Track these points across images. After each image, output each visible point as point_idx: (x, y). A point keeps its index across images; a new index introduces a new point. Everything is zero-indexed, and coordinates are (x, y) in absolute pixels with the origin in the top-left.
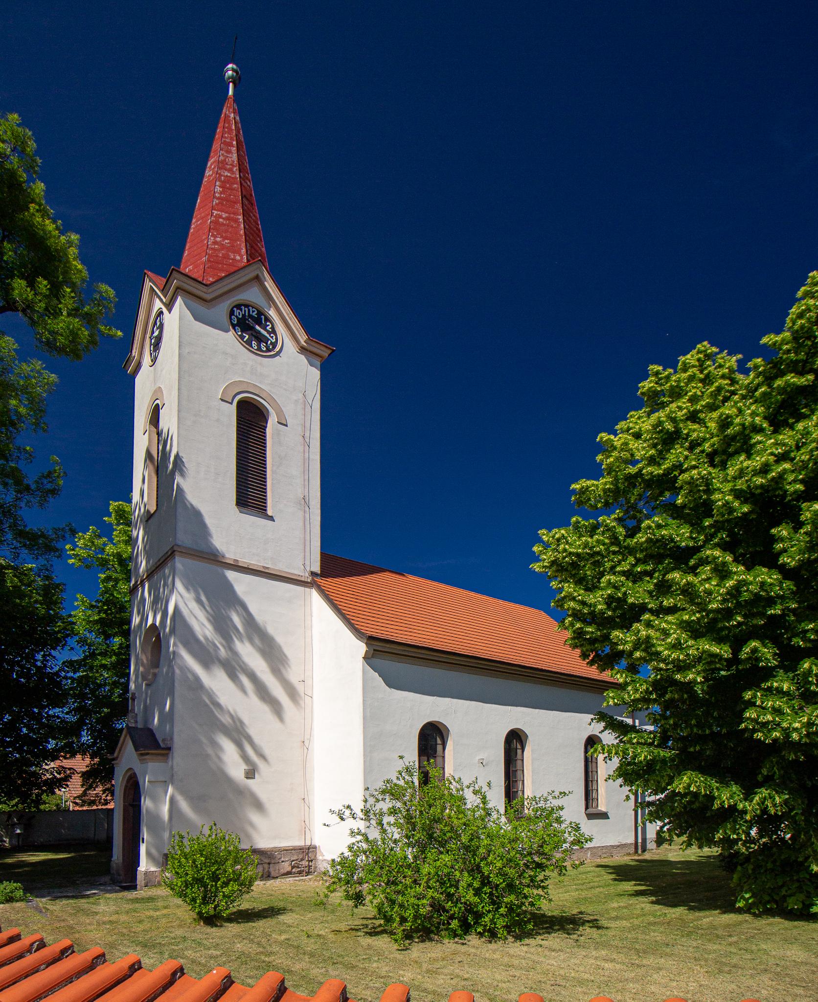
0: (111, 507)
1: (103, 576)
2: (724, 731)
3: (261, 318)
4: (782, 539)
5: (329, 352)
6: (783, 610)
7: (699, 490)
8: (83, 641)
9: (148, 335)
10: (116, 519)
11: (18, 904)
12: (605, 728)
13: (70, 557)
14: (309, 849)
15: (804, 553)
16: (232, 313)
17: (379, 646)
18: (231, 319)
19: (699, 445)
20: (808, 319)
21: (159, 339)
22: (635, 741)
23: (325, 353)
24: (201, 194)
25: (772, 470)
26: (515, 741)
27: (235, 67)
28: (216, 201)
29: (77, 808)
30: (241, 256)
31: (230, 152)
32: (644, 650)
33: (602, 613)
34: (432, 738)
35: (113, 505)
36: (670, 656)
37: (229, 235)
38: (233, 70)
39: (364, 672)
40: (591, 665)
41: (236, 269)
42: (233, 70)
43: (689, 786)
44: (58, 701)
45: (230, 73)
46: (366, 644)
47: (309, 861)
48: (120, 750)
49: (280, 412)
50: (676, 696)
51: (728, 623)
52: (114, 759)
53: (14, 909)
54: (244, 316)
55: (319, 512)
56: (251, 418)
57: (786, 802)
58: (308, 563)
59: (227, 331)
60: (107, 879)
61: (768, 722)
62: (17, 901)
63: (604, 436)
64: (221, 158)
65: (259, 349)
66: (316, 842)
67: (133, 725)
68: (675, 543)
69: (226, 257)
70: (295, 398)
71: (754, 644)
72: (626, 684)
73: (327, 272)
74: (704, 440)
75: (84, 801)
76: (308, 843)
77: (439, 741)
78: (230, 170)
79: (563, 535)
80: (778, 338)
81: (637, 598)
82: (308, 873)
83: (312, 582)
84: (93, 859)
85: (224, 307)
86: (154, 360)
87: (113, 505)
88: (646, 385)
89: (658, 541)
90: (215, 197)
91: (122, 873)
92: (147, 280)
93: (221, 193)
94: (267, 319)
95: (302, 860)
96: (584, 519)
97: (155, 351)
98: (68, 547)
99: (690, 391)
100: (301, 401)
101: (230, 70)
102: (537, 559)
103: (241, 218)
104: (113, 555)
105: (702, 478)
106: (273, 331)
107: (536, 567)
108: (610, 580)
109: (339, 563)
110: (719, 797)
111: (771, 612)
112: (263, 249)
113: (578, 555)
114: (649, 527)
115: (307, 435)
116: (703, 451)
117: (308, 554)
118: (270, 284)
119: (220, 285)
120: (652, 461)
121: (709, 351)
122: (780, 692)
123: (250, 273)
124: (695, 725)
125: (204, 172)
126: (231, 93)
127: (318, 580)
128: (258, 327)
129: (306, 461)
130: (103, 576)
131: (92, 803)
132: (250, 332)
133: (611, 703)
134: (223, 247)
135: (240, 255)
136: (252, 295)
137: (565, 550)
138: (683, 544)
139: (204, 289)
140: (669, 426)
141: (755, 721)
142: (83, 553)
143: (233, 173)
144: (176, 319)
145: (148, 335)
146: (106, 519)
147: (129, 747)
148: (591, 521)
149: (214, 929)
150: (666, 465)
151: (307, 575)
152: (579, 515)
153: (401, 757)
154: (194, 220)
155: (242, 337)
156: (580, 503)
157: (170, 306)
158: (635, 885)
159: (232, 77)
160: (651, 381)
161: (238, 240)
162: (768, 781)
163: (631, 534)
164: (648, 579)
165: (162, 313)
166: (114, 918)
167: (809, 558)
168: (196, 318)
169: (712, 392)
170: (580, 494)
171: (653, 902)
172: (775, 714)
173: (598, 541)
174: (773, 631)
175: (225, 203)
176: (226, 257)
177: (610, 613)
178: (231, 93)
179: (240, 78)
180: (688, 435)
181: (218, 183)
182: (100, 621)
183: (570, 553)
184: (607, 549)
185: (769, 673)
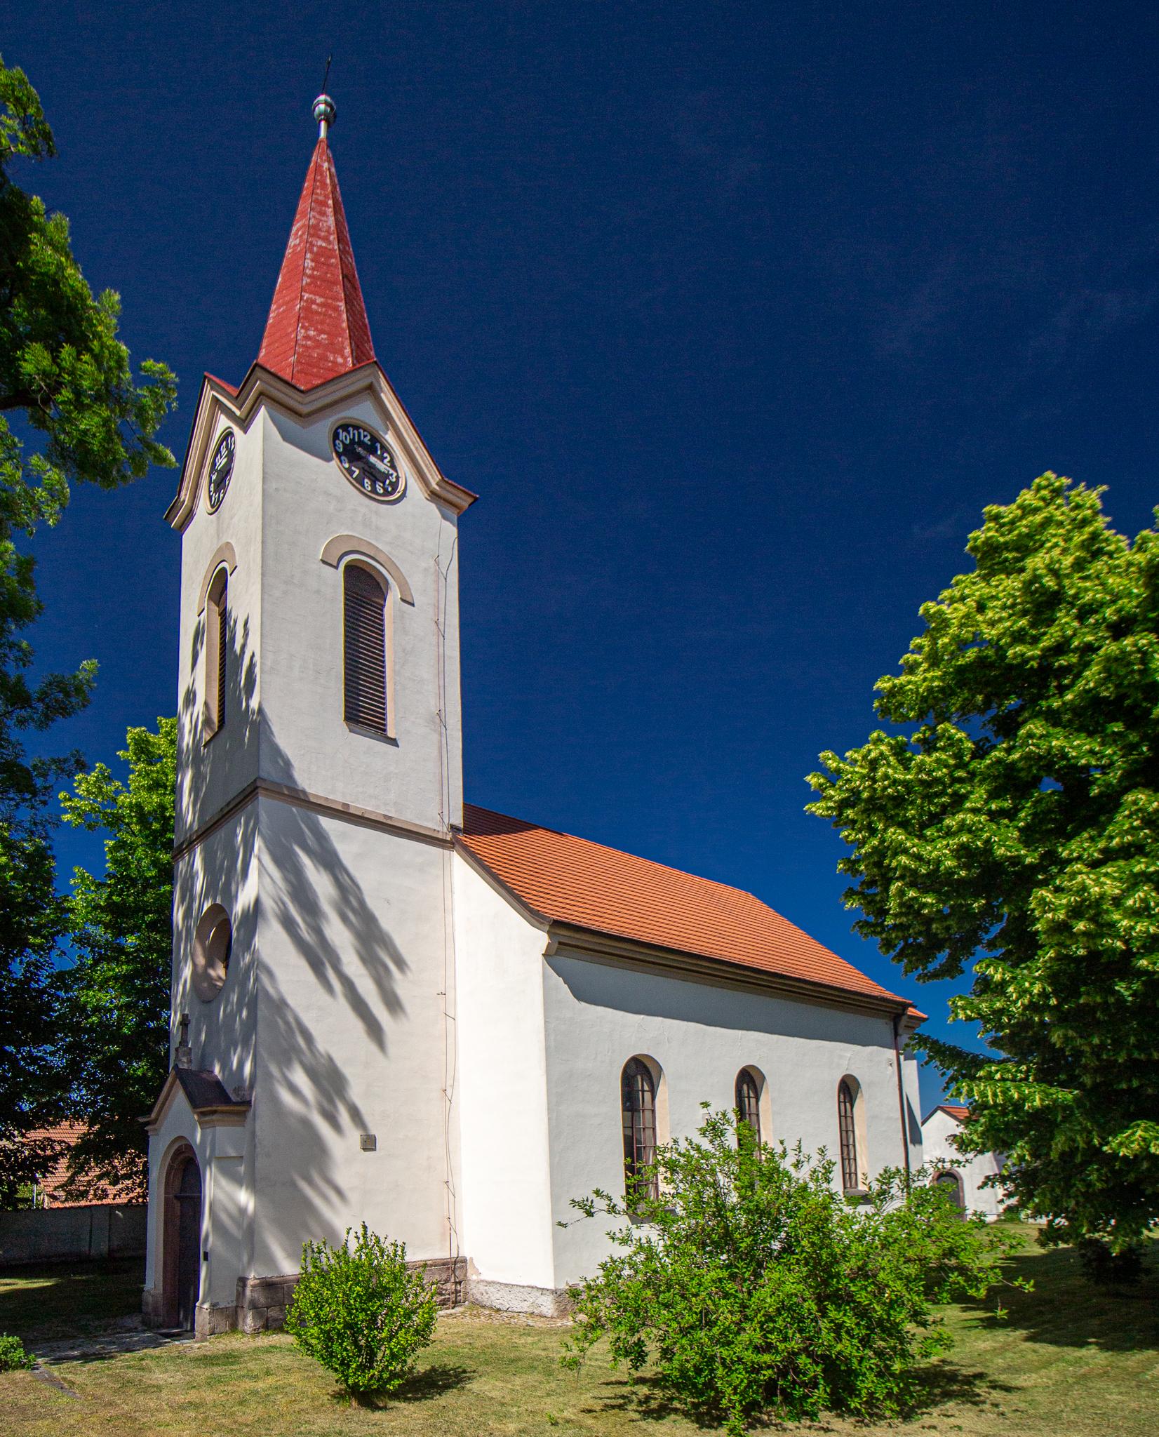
0: (129, 736)
1: (111, 843)
3: (375, 445)
5: (470, 500)
7: (1133, 671)
8: (84, 940)
9: (206, 470)
10: (135, 754)
11: (19, 1374)
13: (65, 811)
14: (455, 1263)
16: (336, 436)
21: (226, 472)
22: (998, 1076)
23: (465, 502)
27: (329, 99)
28: (306, 280)
29: (57, 1205)
30: (345, 359)
31: (323, 214)
32: (1090, 920)
33: (950, 872)
35: (133, 733)
36: (1132, 928)
37: (326, 328)
38: (326, 103)
40: (899, 961)
44: (44, 1034)
45: (322, 107)
46: (548, 932)
47: (456, 1283)
48: (164, 1104)
49: (404, 586)
50: (1098, 999)
52: (148, 1123)
53: (14, 1383)
54: (352, 441)
55: (459, 735)
56: (364, 590)
59: (328, 460)
60: (134, 1321)
62: (15, 1368)
64: (312, 221)
65: (374, 491)
66: (466, 1252)
67: (186, 1066)
68: (1069, 760)
69: (323, 358)
70: (424, 565)
72: (1003, 984)
74: (1102, 604)
75: (69, 1193)
76: (454, 1255)
78: (326, 239)
79: (882, 754)
82: (456, 1303)
84: (110, 1292)
85: (323, 429)
86: (216, 505)
87: (133, 733)
88: (979, 536)
89: (1040, 757)
90: (304, 274)
91: (162, 1310)
92: (207, 387)
93: (313, 269)
94: (385, 449)
95: (447, 1281)
96: (889, 735)
97: (217, 490)
98: (62, 795)
99: (1048, 540)
100: (432, 570)
101: (321, 104)
102: (817, 796)
103: (342, 305)
104: (131, 807)
105: (1139, 650)
106: (393, 467)
107: (817, 808)
108: (964, 820)
115: (441, 620)
117: (445, 798)
118: (388, 398)
119: (330, 389)
120: (1019, 637)
121: (1057, 484)
123: (361, 380)
124: (1134, 1046)
126: (323, 134)
127: (461, 836)
128: (373, 459)
129: (441, 659)
130: (111, 843)
131: (84, 1194)
132: (360, 464)
133: (961, 1016)
134: (318, 344)
135: (343, 356)
136: (363, 412)
137: (886, 777)
138: (1083, 761)
139: (297, 396)
140: (1049, 582)
142: (83, 805)
144: (256, 443)
145: (206, 470)
146: (120, 753)
147: (179, 1100)
148: (900, 738)
149: (378, 1415)
150: (1045, 643)
152: (882, 729)
154: (273, 307)
155: (351, 473)
156: (885, 710)
157: (245, 423)
159: (325, 113)
160: (989, 529)
161: (340, 335)
163: (979, 753)
164: (1006, 821)
165: (231, 434)
166: (193, 1396)
168: (286, 438)
169: (1083, 541)
170: (888, 697)
171: (1027, 1339)
173: (938, 761)
175: (319, 284)
176: (323, 358)
177: (963, 873)
178: (323, 134)
179: (335, 116)
180: (1076, 597)
181: (308, 256)
182: (111, 907)
184: (950, 775)
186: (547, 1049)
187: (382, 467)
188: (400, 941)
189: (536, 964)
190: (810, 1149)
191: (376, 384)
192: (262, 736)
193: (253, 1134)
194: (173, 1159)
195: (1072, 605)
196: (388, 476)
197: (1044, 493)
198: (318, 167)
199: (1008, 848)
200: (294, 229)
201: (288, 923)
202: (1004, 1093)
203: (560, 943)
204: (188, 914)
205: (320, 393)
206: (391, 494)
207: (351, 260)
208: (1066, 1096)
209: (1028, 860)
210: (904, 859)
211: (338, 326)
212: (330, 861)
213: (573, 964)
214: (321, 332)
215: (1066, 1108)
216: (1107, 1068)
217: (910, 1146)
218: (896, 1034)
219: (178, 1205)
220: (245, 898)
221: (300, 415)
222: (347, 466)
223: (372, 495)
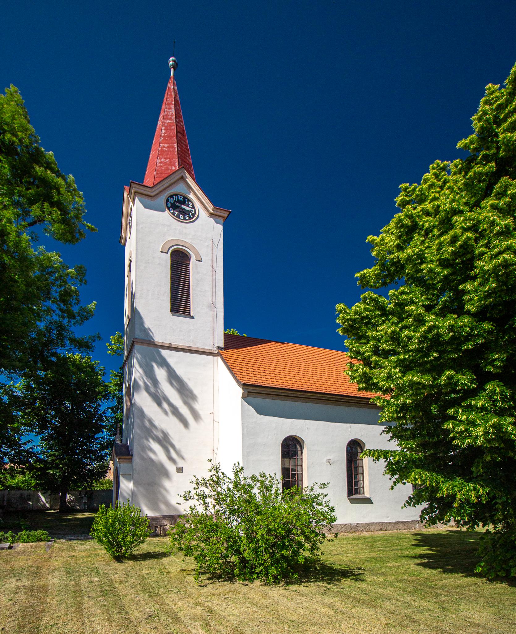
3: (185, 200)
5: (228, 213)
6: (474, 345)
15: (481, 301)
16: (167, 201)
17: (251, 389)
18: (167, 204)
20: (485, 121)
23: (225, 214)
24: (155, 136)
25: (458, 240)
28: (162, 139)
34: (291, 448)
37: (168, 156)
38: (173, 61)
39: (242, 406)
41: (166, 175)
42: (173, 61)
45: (171, 63)
51: (428, 358)
55: (222, 310)
56: (180, 260)
58: (215, 342)
59: (163, 211)
63: (370, 238)
64: (166, 113)
65: (185, 219)
70: (207, 244)
71: (448, 373)
77: (299, 448)
78: (171, 119)
80: (467, 141)
83: (217, 353)
90: (161, 136)
93: (165, 133)
94: (189, 200)
100: (211, 245)
103: (176, 145)
105: (416, 254)
106: (193, 207)
109: (238, 339)
111: (464, 347)
112: (190, 160)
113: (353, 320)
115: (214, 265)
117: (215, 336)
118: (189, 180)
125: (157, 123)
128: (183, 206)
129: (214, 281)
132: (178, 210)
134: (165, 164)
136: (179, 188)
137: (344, 318)
139: (149, 190)
140: (407, 222)
151: (215, 349)
153: (210, 461)
155: (173, 214)
158: (428, 550)
159: (172, 65)
167: (484, 304)
168: (146, 207)
175: (167, 138)
179: (177, 64)
181: (163, 128)
183: (348, 319)
188: (196, 392)
189: (239, 399)
191: (184, 175)
195: (422, 229)
198: (170, 88)
201: (147, 389)
203: (248, 392)
205: (158, 187)
206: (192, 218)
212: (164, 363)
222: (172, 212)
223: (184, 221)
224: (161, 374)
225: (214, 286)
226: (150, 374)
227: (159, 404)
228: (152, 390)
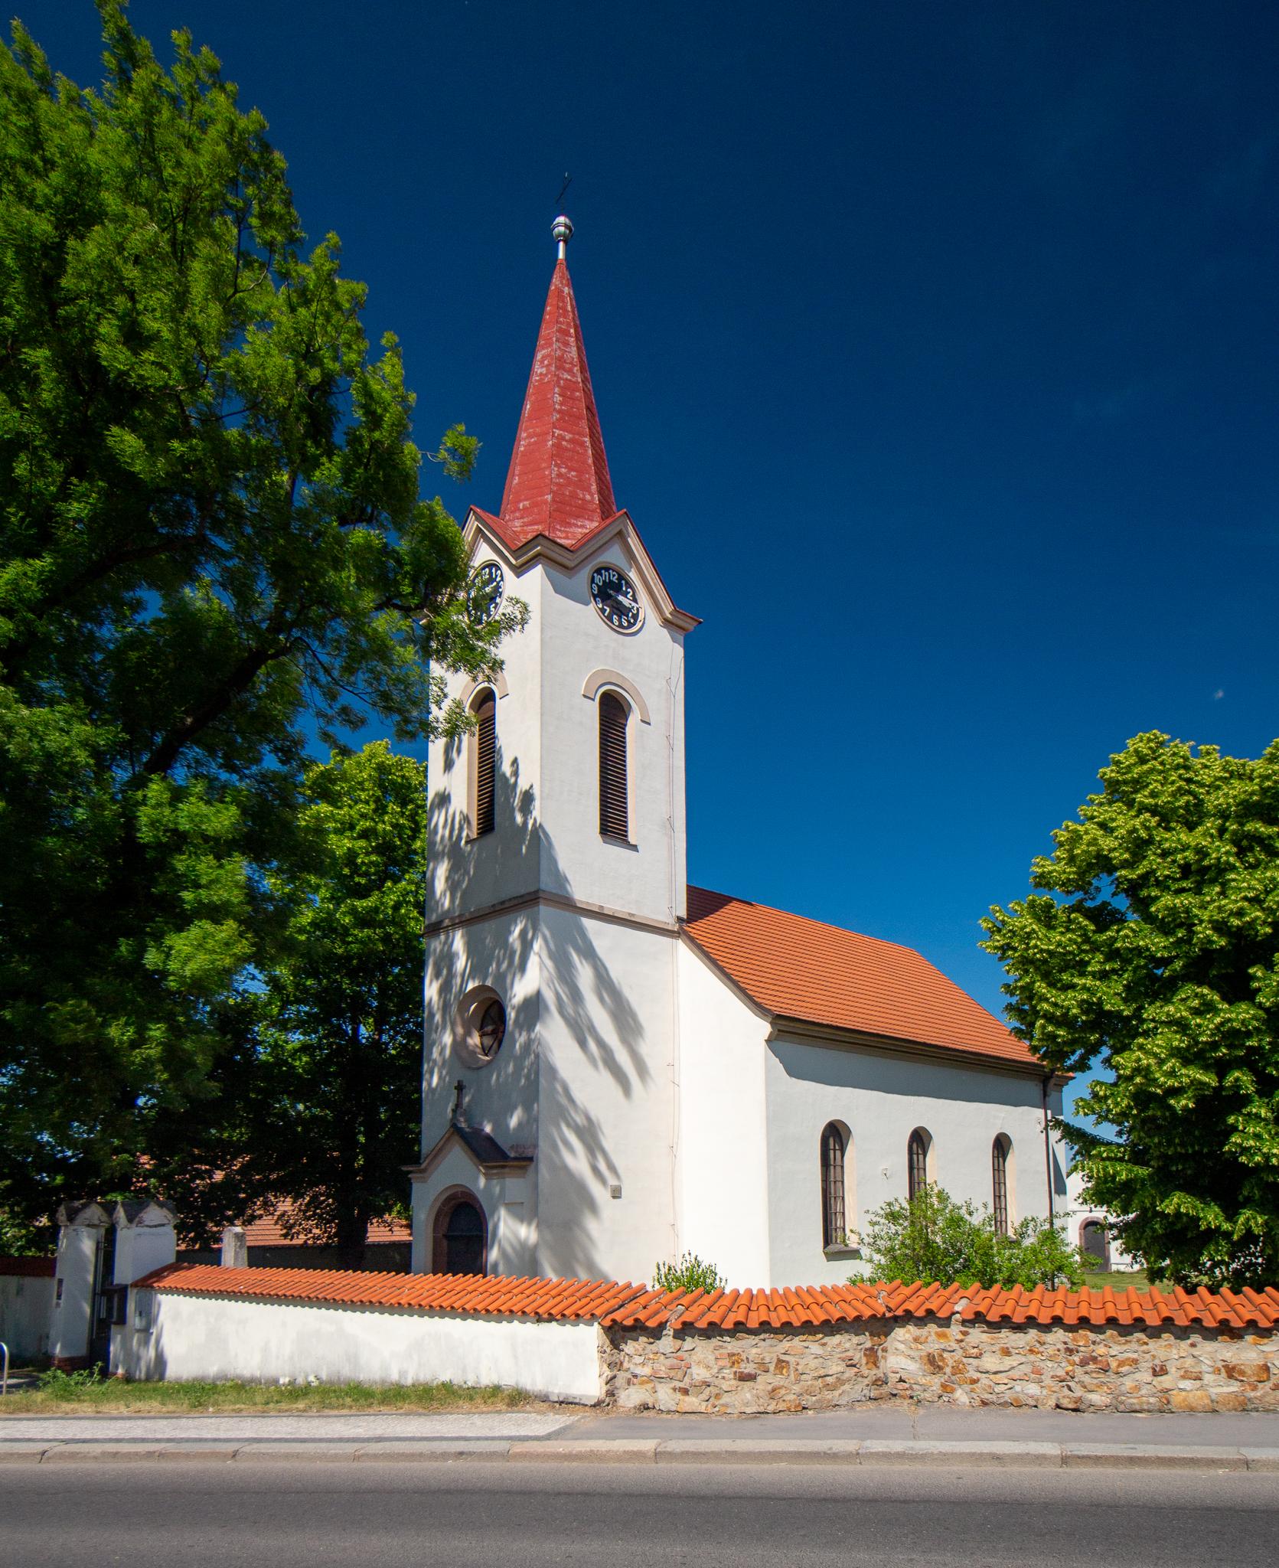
2: (1205, 1150)
4: (1258, 979)
12: (1063, 1137)
19: (1171, 854)
26: (919, 1141)
30: (592, 495)
31: (566, 344)
38: (566, 226)
39: (767, 1059)
43: (1179, 1206)
45: (562, 229)
49: (644, 709)
56: (613, 711)
57: (1266, 1223)
59: (587, 604)
61: (1251, 1147)
73: (689, 516)
78: (570, 371)
81: (1113, 1005)
85: (585, 573)
93: (561, 404)
94: (629, 585)
103: (587, 439)
106: (635, 600)
110: (1205, 1218)
114: (1127, 936)
116: (1174, 861)
122: (1258, 1116)
126: (561, 255)
128: (621, 598)
129: (671, 768)
136: (613, 556)
137: (1036, 946)
140: (1143, 834)
141: (1240, 1145)
143: (574, 375)
144: (527, 588)
155: (603, 611)
159: (564, 235)
162: (1247, 1202)
172: (1254, 1137)
173: (1070, 940)
174: (1251, 1061)
175: (567, 419)
176: (574, 496)
178: (561, 255)
181: (557, 390)
185: (1246, 1100)
186: (768, 1118)
187: (625, 601)
188: (642, 1017)
189: (761, 1049)
190: (976, 1204)
192: (543, 853)
193: (536, 1186)
194: (444, 1204)
196: (630, 610)
197: (1152, 745)
199: (1113, 1005)
200: (539, 356)
202: (1104, 1169)
204: (445, 989)
207: (590, 386)
208: (1143, 1172)
209: (1125, 1013)
210: (1045, 1006)
211: (584, 462)
212: (589, 953)
213: (785, 1046)
214: (571, 469)
215: (1143, 1180)
216: (1164, 1157)
217: (1055, 1197)
218: (1045, 1095)
219: (445, 1243)
220: (521, 989)
221: (566, 567)
224: (585, 976)
225: (671, 782)
226: (564, 972)
227: (582, 1044)
228: (570, 1010)
